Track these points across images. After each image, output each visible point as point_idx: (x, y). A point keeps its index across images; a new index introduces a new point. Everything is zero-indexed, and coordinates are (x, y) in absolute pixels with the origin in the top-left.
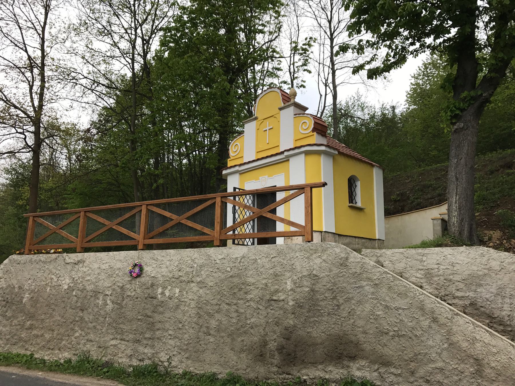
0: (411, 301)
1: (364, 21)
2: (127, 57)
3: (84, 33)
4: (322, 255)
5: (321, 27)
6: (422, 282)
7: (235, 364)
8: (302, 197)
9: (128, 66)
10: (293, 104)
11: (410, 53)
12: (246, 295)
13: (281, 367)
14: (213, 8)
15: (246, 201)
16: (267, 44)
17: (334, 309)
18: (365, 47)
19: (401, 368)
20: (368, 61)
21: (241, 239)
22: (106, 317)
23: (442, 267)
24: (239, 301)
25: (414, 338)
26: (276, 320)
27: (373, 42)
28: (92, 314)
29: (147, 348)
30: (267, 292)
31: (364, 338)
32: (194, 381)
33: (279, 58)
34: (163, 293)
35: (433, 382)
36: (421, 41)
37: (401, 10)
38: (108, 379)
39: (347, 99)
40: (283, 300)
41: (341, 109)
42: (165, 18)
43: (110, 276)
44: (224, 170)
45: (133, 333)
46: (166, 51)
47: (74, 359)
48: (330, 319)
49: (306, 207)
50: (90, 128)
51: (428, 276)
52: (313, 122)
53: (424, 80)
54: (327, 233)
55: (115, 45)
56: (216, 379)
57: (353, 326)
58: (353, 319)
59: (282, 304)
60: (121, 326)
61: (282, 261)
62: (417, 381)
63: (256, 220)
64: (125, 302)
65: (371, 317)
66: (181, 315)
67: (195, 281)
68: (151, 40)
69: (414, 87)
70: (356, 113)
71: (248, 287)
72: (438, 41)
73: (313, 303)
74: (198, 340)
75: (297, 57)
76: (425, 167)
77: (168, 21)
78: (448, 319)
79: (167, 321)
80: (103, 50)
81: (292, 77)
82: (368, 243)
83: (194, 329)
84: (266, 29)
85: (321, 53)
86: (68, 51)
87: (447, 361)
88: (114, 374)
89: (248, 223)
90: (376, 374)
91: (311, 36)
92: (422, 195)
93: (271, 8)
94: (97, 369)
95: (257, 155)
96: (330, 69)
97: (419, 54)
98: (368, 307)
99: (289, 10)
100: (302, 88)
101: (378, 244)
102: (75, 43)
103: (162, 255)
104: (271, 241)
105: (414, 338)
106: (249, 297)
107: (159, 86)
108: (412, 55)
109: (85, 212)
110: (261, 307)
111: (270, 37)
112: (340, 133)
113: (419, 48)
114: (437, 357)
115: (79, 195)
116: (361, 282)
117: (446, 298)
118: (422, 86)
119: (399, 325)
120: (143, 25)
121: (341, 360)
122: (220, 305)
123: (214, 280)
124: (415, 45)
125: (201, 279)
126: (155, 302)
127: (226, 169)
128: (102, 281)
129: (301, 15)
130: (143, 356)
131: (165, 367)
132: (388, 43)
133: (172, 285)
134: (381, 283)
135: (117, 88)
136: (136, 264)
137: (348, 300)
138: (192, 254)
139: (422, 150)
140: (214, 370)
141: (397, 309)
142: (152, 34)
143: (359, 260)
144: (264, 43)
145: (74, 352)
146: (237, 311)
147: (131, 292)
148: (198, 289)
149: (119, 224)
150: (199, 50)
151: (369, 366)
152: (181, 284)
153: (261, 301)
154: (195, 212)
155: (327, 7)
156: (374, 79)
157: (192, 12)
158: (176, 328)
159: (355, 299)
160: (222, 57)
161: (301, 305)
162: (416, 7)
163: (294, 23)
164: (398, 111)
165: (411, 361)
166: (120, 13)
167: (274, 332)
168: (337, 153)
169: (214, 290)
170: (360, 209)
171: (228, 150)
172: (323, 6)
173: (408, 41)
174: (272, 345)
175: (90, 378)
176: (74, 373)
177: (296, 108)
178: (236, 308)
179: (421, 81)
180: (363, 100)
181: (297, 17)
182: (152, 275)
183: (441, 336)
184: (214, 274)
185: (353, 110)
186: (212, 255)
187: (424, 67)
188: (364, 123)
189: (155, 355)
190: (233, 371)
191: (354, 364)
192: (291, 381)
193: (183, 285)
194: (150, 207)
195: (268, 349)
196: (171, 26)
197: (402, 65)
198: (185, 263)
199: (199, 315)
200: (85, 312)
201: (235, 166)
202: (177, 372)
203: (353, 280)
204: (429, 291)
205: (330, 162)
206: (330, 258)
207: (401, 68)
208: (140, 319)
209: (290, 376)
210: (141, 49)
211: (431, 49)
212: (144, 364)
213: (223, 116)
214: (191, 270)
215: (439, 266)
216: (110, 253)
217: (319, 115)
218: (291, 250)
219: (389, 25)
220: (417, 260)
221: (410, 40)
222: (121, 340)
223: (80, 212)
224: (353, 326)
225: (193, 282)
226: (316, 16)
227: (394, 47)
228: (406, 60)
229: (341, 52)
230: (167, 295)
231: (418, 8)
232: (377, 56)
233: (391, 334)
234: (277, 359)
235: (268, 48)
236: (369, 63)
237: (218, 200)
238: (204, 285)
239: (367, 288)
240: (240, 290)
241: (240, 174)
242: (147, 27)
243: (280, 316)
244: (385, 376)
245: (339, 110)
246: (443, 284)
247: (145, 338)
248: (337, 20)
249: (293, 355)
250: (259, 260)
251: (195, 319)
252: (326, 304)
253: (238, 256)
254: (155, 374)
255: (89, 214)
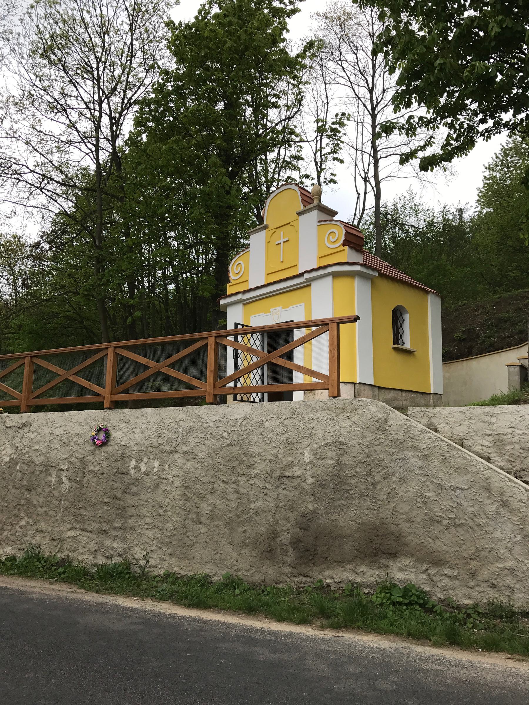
0: (473, 479)
1: (416, 90)
2: (89, 142)
3: (30, 109)
4: (353, 415)
5: (359, 98)
6: (490, 451)
7: (235, 562)
8: (325, 337)
9: (91, 154)
10: (316, 206)
11: (479, 135)
12: (249, 470)
13: (297, 566)
14: (208, 73)
15: (252, 341)
16: (283, 123)
17: (367, 489)
18: (417, 126)
19: (458, 568)
20: (421, 147)
21: (245, 394)
22: (61, 500)
23: (518, 432)
24: (239, 478)
25: (476, 528)
26: (289, 503)
27: (429, 119)
28: (42, 496)
29: (116, 541)
30: (278, 466)
31: (409, 528)
32: (179, 586)
33: (299, 142)
34: (137, 467)
35: (502, 586)
36: (495, 117)
37: (467, 73)
38: (65, 582)
39: (395, 200)
40: (300, 477)
41: (387, 213)
42: (141, 87)
43: (66, 444)
44: (222, 298)
45: (98, 520)
46: (144, 133)
47: (20, 555)
48: (362, 502)
49: (330, 350)
50: (40, 241)
51: (498, 443)
52: (344, 232)
53: (502, 173)
54: (362, 386)
55: (72, 125)
56: (208, 582)
57: (394, 512)
58: (394, 502)
59: (297, 482)
60: (82, 511)
61: (298, 423)
62: (480, 585)
63: (266, 366)
64: (86, 480)
65: (419, 500)
66: (162, 496)
67: (180, 451)
68: (122, 118)
69: (488, 182)
70: (407, 218)
71: (252, 459)
72: (520, 116)
73: (340, 480)
74: (185, 531)
75: (325, 141)
76: (502, 293)
77: (144, 91)
78: (523, 503)
79: (143, 504)
80: (57, 133)
81: (319, 169)
82: (421, 399)
83: (180, 516)
84: (281, 102)
85: (359, 135)
86: (8, 134)
87: (520, 559)
88: (72, 576)
89: (255, 372)
90: (424, 576)
91: (344, 111)
92: (496, 332)
93: (288, 72)
94: (51, 569)
95: (267, 279)
96: (371, 158)
97: (492, 135)
98: (413, 486)
99: (314, 74)
100: (332, 183)
101: (433, 400)
102: (16, 123)
103: (136, 415)
104: (287, 396)
105: (476, 528)
106: (253, 472)
107: (134, 182)
108: (482, 138)
109: (31, 357)
110: (269, 486)
111: (288, 113)
112: (385, 246)
113: (493, 127)
114: (507, 554)
115: (28, 333)
116: (405, 452)
117: (522, 474)
118: (500, 180)
119: (455, 511)
120: (110, 97)
121: (377, 558)
122: (214, 483)
123: (206, 449)
124: (487, 122)
125: (189, 448)
126: (126, 479)
127: (225, 298)
128: (56, 452)
129: (331, 81)
130: (111, 551)
131: (140, 566)
132: (449, 120)
133: (149, 456)
134: (431, 454)
135: (74, 186)
136: (100, 428)
137: (387, 476)
138: (176, 415)
139: (498, 270)
140: (207, 571)
141: (454, 489)
142: (122, 110)
143: (402, 422)
144: (279, 120)
145: (19, 546)
146: (237, 491)
147: (95, 466)
148: (185, 461)
149: (171, 366)
150: (188, 132)
151: (415, 565)
152: (161, 455)
153: (269, 477)
154: (180, 357)
155: (367, 69)
156: (429, 171)
157: (178, 78)
158: (155, 514)
159: (396, 475)
160: (219, 142)
161: (324, 483)
162: (487, 68)
163: (322, 94)
164: (467, 216)
165: (472, 559)
166: (78, 80)
167: (287, 520)
168: (377, 274)
169: (206, 464)
170: (409, 352)
171: (228, 271)
172: (362, 69)
173: (477, 117)
174: (284, 538)
175: (40, 580)
176: (19, 574)
177: (320, 213)
178: (236, 487)
179: (498, 173)
180: (417, 200)
181: (326, 84)
182: (123, 443)
183: (512, 526)
184: (206, 442)
185: (403, 215)
186: (203, 416)
187: (502, 154)
188: (419, 233)
189: (127, 550)
190: (232, 572)
191: (395, 563)
192: (309, 586)
193: (165, 456)
194: (118, 351)
195: (278, 543)
196: (150, 97)
197: (469, 152)
198: (166, 426)
199: (185, 497)
200: (33, 492)
201: (237, 293)
202: (156, 573)
203: (394, 450)
204: (499, 464)
205: (367, 287)
206: (364, 420)
207: (466, 155)
208: (107, 502)
209: (308, 579)
210: (108, 131)
211: (508, 129)
212: (113, 562)
213: (221, 223)
214: (175, 436)
215: (514, 430)
216: (66, 413)
217: (356, 223)
218: (310, 409)
219: (451, 95)
220: (484, 422)
221: (480, 116)
222: (82, 530)
223: (25, 357)
224: (394, 512)
225: (177, 452)
226: (351, 83)
227: (457, 126)
228: (474, 144)
229: (384, 135)
230: (143, 469)
231: (490, 70)
232: (434, 138)
233: (445, 522)
234: (291, 557)
235: (284, 129)
236: (422, 148)
237: (211, 341)
238: (193, 456)
239: (413, 460)
240: (242, 462)
241: (244, 304)
242: (116, 100)
243: (295, 499)
244: (436, 579)
245: (384, 215)
246: (519, 454)
247: (114, 528)
248: (381, 89)
249: (313, 550)
250: (266, 423)
251: (181, 503)
252: (357, 483)
253: (239, 417)
254: (127, 576)
255: (36, 361)
